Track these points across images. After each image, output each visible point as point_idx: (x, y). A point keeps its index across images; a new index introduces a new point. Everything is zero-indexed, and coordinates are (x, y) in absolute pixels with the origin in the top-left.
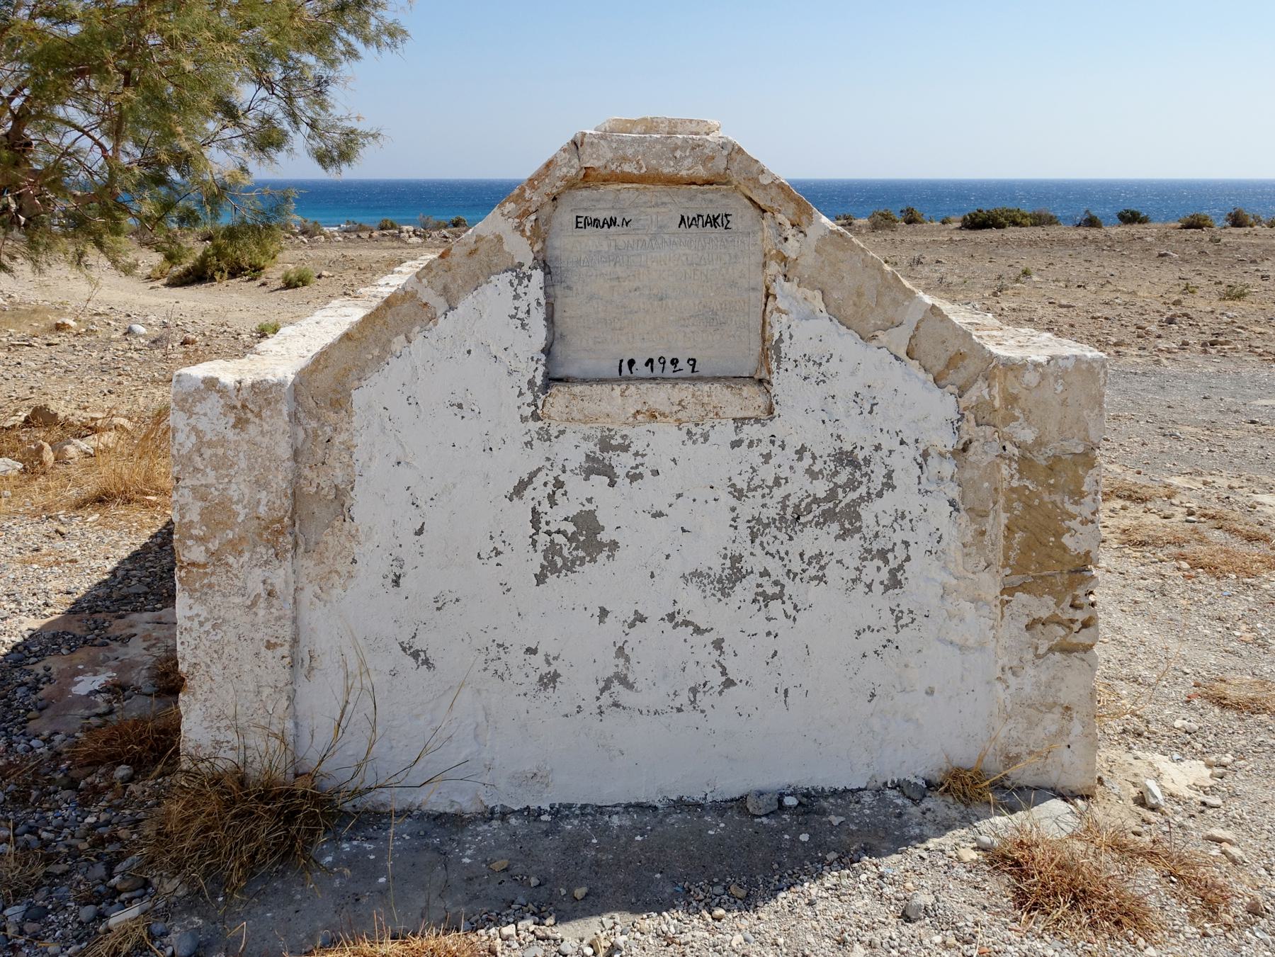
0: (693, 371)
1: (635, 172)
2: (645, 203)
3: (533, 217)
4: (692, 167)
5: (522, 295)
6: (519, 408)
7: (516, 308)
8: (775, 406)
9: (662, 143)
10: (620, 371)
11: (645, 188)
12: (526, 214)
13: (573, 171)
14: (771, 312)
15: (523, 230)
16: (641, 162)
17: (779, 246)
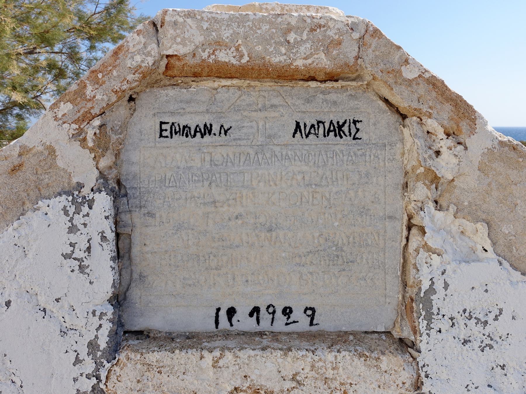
0: (311, 324)
1: (234, 61)
2: (249, 105)
3: (97, 122)
4: (312, 54)
5: (81, 227)
6: (75, 380)
7: (72, 245)
8: (424, 380)
9: (271, 23)
10: (217, 323)
11: (249, 86)
12: (88, 118)
13: (150, 61)
14: (417, 251)
15: (85, 140)
16: (242, 48)
17: (430, 162)
